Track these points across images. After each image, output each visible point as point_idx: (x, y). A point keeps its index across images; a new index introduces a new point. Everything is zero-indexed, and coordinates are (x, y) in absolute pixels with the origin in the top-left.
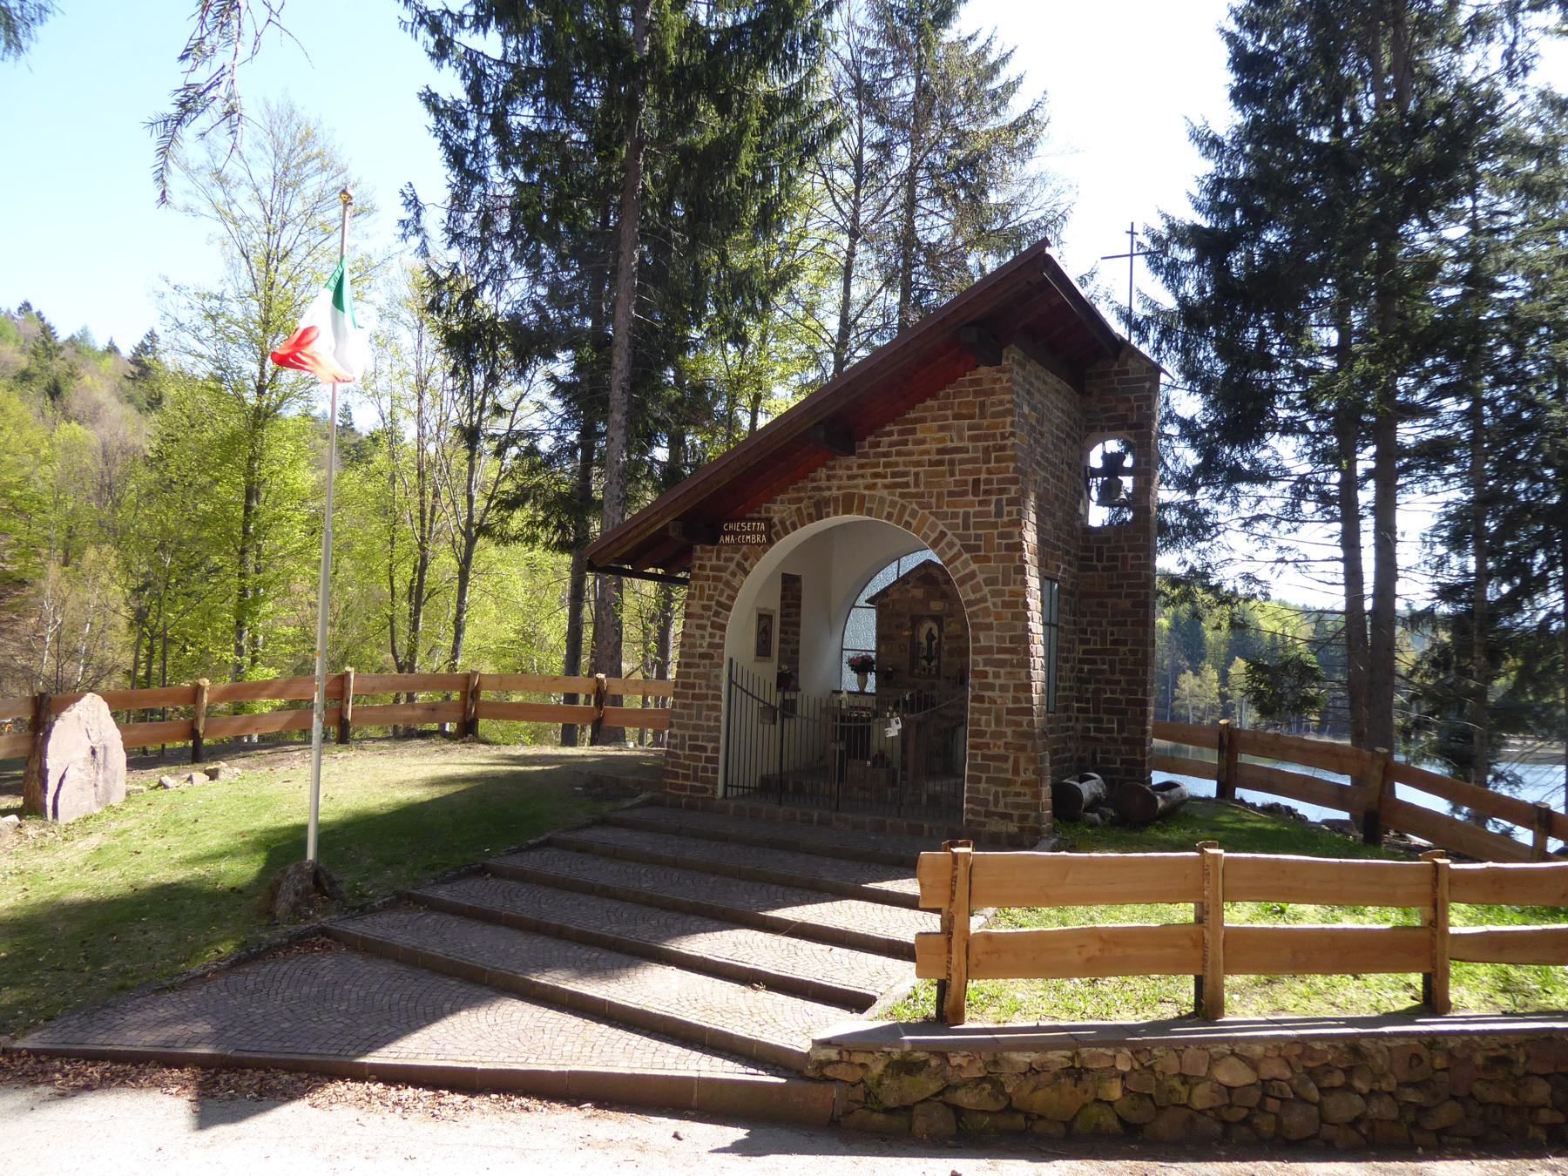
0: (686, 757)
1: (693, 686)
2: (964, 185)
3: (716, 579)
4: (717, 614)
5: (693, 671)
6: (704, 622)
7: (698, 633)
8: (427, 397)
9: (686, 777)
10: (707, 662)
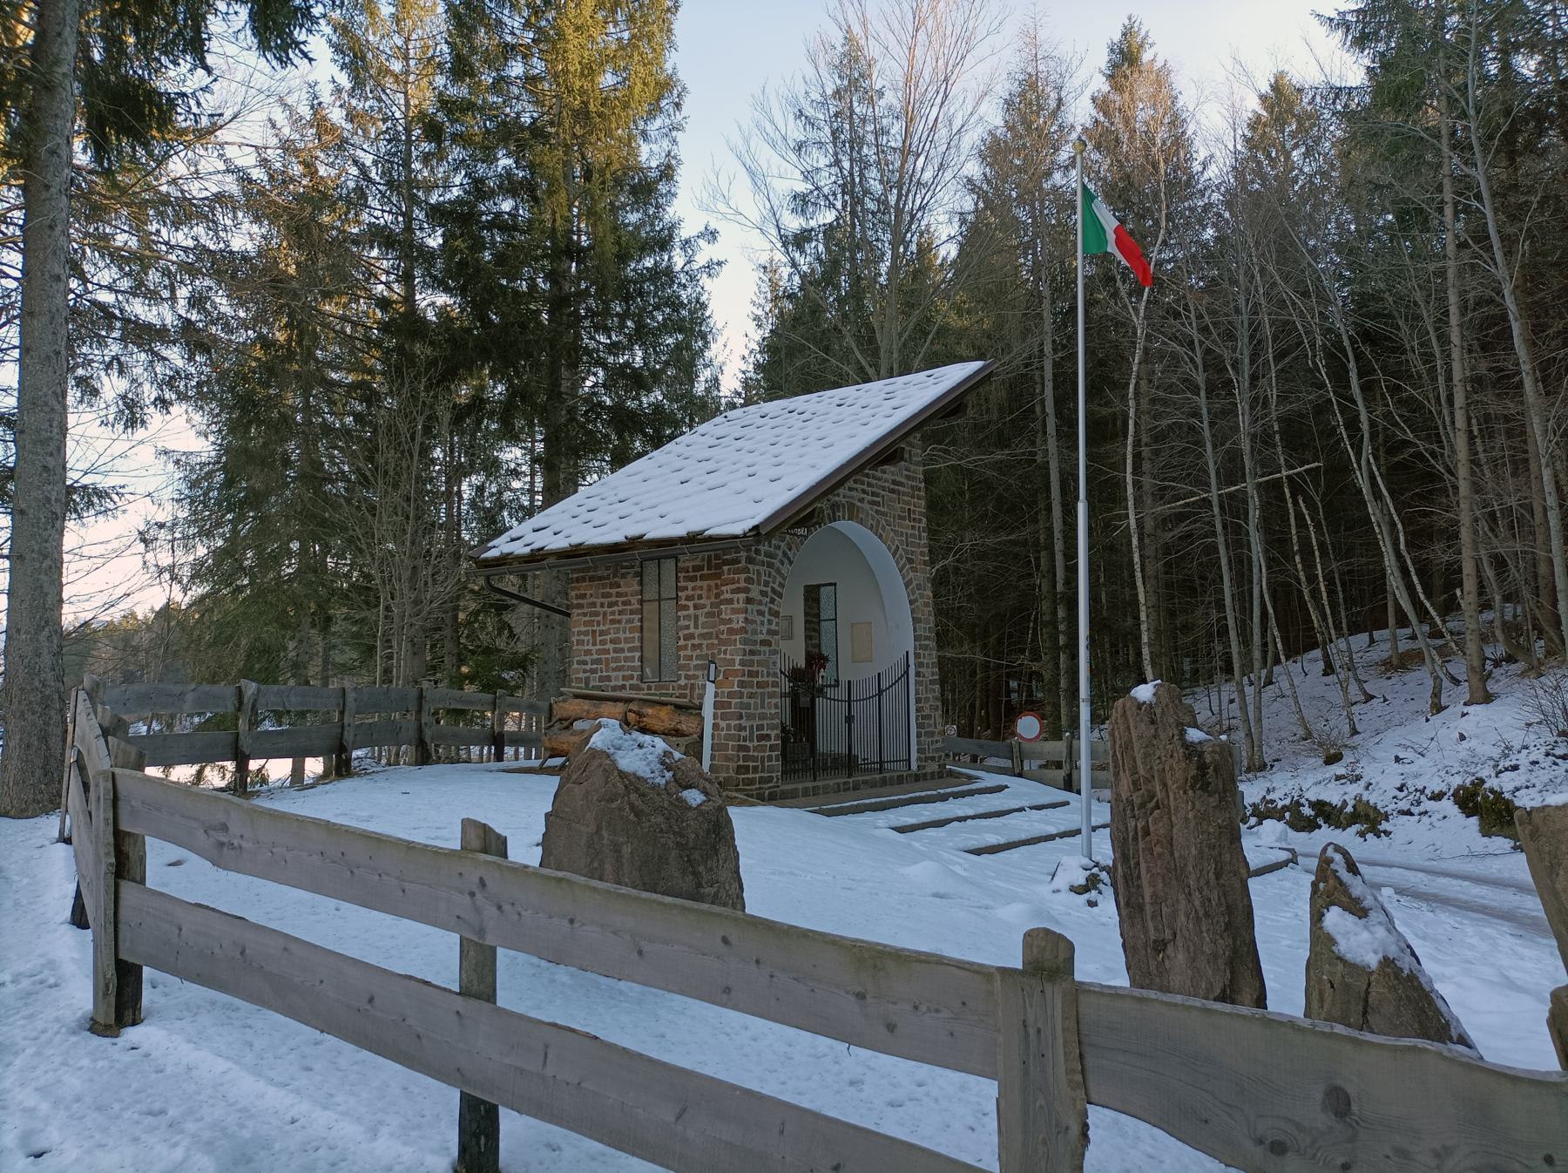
0: (755, 748)
1: (756, 674)
2: (1020, 170)
3: (770, 565)
4: (773, 601)
5: (756, 658)
6: (762, 608)
7: (759, 619)
8: (921, 36)
9: (755, 769)
10: (766, 649)
